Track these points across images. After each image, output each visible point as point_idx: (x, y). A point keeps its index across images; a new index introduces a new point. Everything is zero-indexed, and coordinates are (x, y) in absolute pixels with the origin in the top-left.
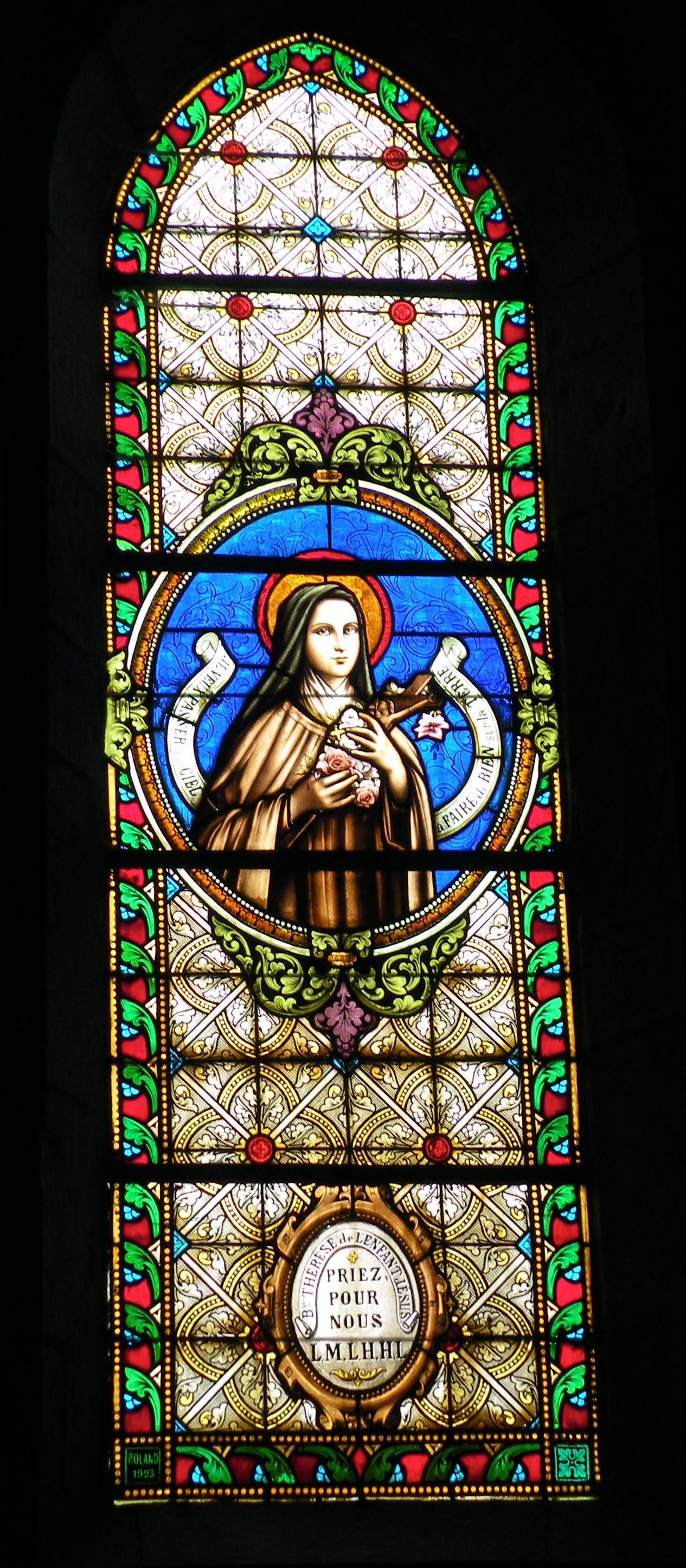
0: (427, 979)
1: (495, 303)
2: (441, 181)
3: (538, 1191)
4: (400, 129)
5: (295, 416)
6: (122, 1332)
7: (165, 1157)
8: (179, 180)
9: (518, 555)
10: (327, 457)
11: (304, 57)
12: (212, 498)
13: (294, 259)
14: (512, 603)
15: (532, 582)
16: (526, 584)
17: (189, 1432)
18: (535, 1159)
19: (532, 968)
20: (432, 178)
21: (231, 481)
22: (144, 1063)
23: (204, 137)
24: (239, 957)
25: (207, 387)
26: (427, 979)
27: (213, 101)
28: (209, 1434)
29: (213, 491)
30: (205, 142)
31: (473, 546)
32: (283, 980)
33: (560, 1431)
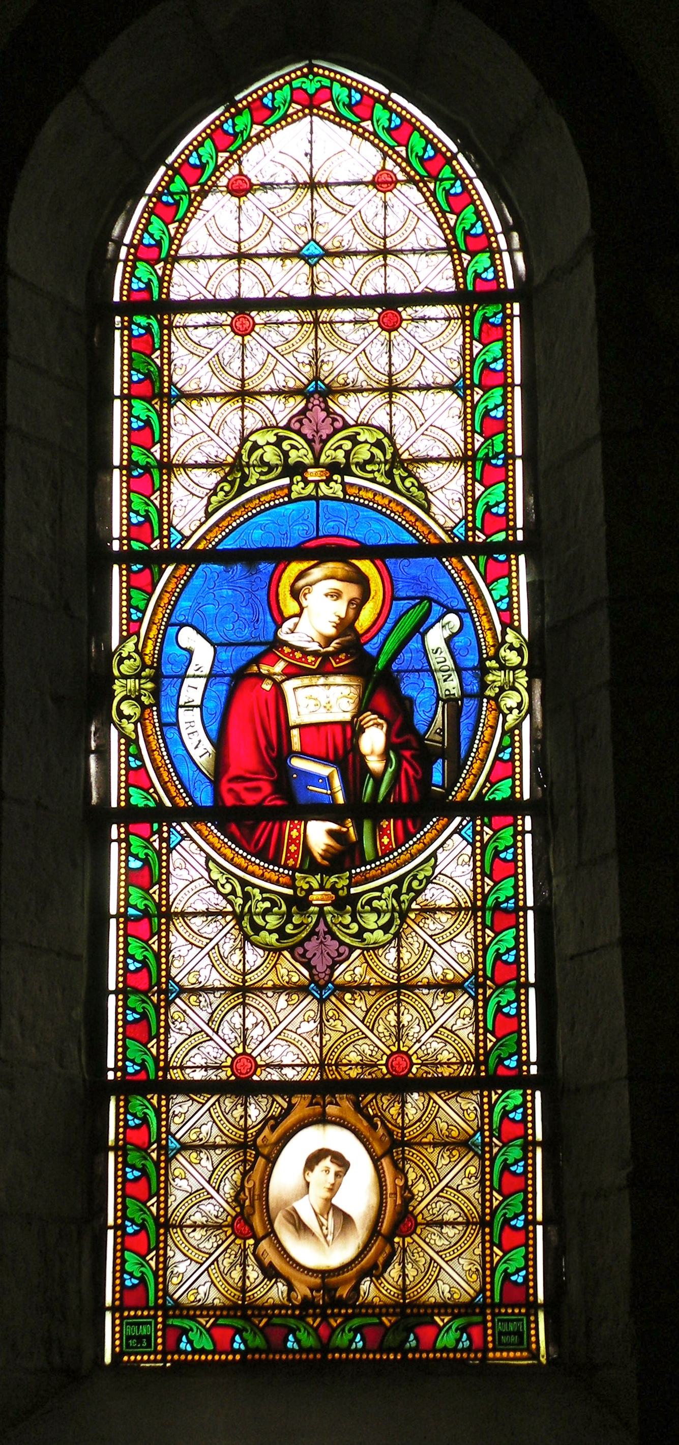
0: (396, 915)
1: (475, 306)
2: (427, 200)
3: (490, 1097)
4: (390, 152)
5: (290, 420)
6: (123, 1222)
7: (160, 1073)
8: (189, 215)
9: (487, 538)
10: (317, 458)
11: (305, 91)
12: (214, 499)
13: (293, 280)
14: (484, 578)
15: (502, 557)
16: (496, 560)
17: (177, 1305)
18: (486, 1071)
19: (490, 902)
20: (419, 198)
21: (232, 483)
22: (145, 993)
23: (213, 174)
24: (231, 897)
25: (205, 419)
26: (396, 915)
27: (222, 138)
28: (195, 1308)
29: (215, 494)
30: (214, 179)
31: (446, 532)
32: (268, 918)
33: (500, 1305)
